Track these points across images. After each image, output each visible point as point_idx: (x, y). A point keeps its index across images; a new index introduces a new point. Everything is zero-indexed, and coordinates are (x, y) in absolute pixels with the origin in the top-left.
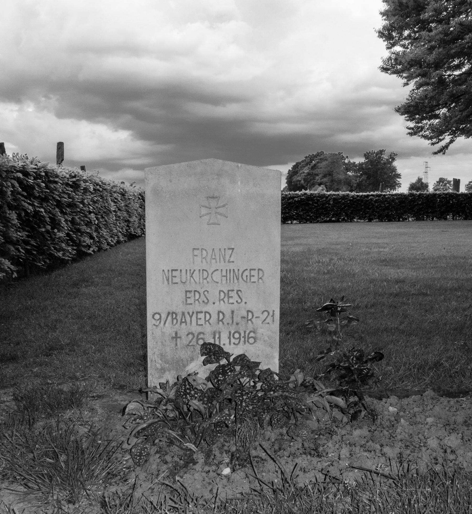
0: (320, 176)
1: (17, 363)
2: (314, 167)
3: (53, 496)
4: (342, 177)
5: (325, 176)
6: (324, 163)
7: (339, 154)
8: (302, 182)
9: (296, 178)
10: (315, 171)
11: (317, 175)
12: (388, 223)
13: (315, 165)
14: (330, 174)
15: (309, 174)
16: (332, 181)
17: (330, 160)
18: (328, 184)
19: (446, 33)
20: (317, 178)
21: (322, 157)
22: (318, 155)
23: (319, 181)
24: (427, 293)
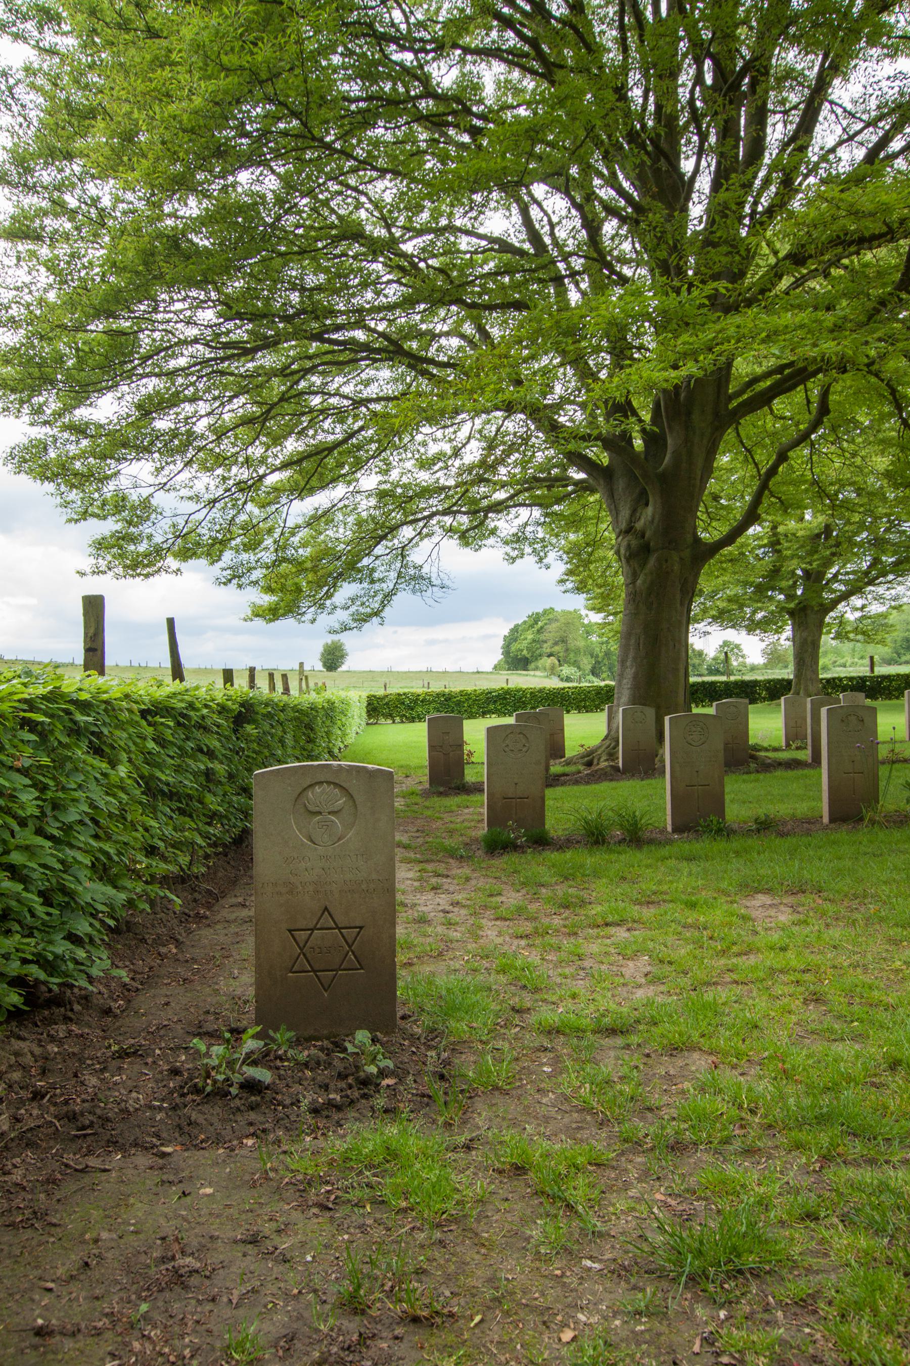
0: (549, 644)
1: (585, 819)
2: (539, 631)
3: (536, 1299)
4: (581, 644)
5: (556, 644)
6: (554, 625)
7: (575, 611)
8: (525, 652)
9: (514, 647)
10: (542, 637)
11: (546, 642)
12: (761, 776)
13: (542, 628)
14: (563, 640)
15: (534, 641)
16: (567, 650)
17: (562, 620)
18: (561, 654)
19: (437, 237)
20: (545, 645)
21: (551, 616)
22: (545, 612)
23: (548, 650)
24: (467, 317)
